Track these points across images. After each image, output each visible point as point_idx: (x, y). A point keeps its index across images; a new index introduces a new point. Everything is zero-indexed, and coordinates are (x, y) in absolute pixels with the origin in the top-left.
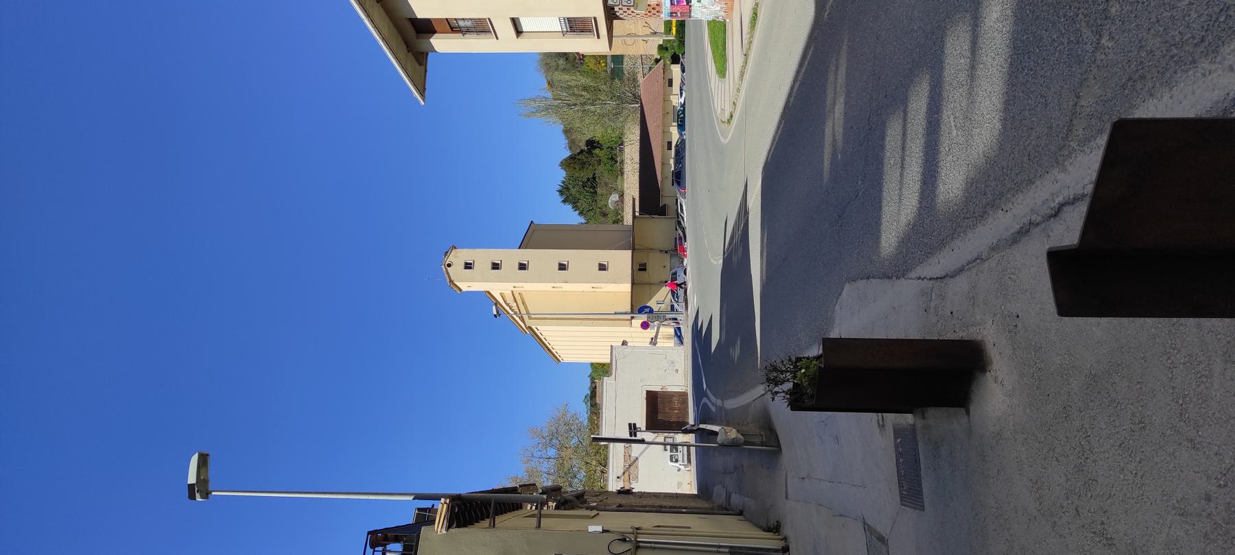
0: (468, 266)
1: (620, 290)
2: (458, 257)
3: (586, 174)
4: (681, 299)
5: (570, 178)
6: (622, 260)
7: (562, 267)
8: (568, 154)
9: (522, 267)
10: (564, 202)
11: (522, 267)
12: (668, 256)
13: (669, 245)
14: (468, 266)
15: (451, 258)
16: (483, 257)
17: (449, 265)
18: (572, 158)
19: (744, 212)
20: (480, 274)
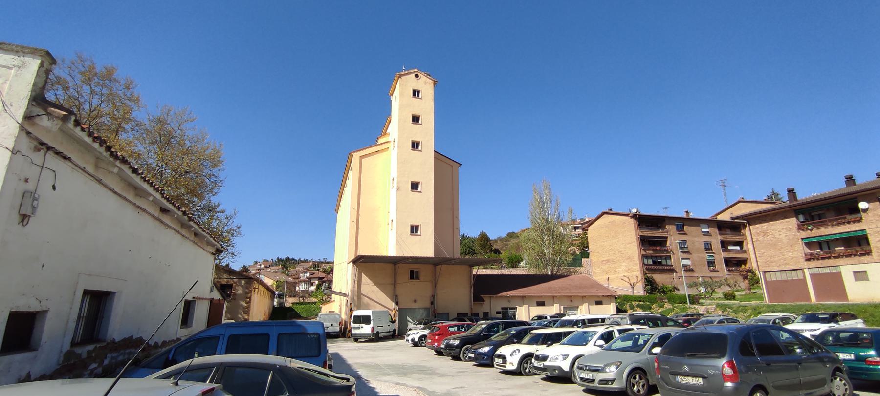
0: (416, 93)
1: (388, 245)
2: (425, 84)
3: (477, 248)
4: (372, 303)
5: (473, 240)
6: (423, 247)
7: (415, 186)
8: (492, 236)
9: (415, 145)
10: (98, 302)
11: (415, 145)
12: (428, 305)
13: (441, 307)
14: (416, 93)
15: (423, 78)
16: (426, 106)
17: (417, 76)
18: (488, 239)
19: (166, 377)
20: (411, 101)
